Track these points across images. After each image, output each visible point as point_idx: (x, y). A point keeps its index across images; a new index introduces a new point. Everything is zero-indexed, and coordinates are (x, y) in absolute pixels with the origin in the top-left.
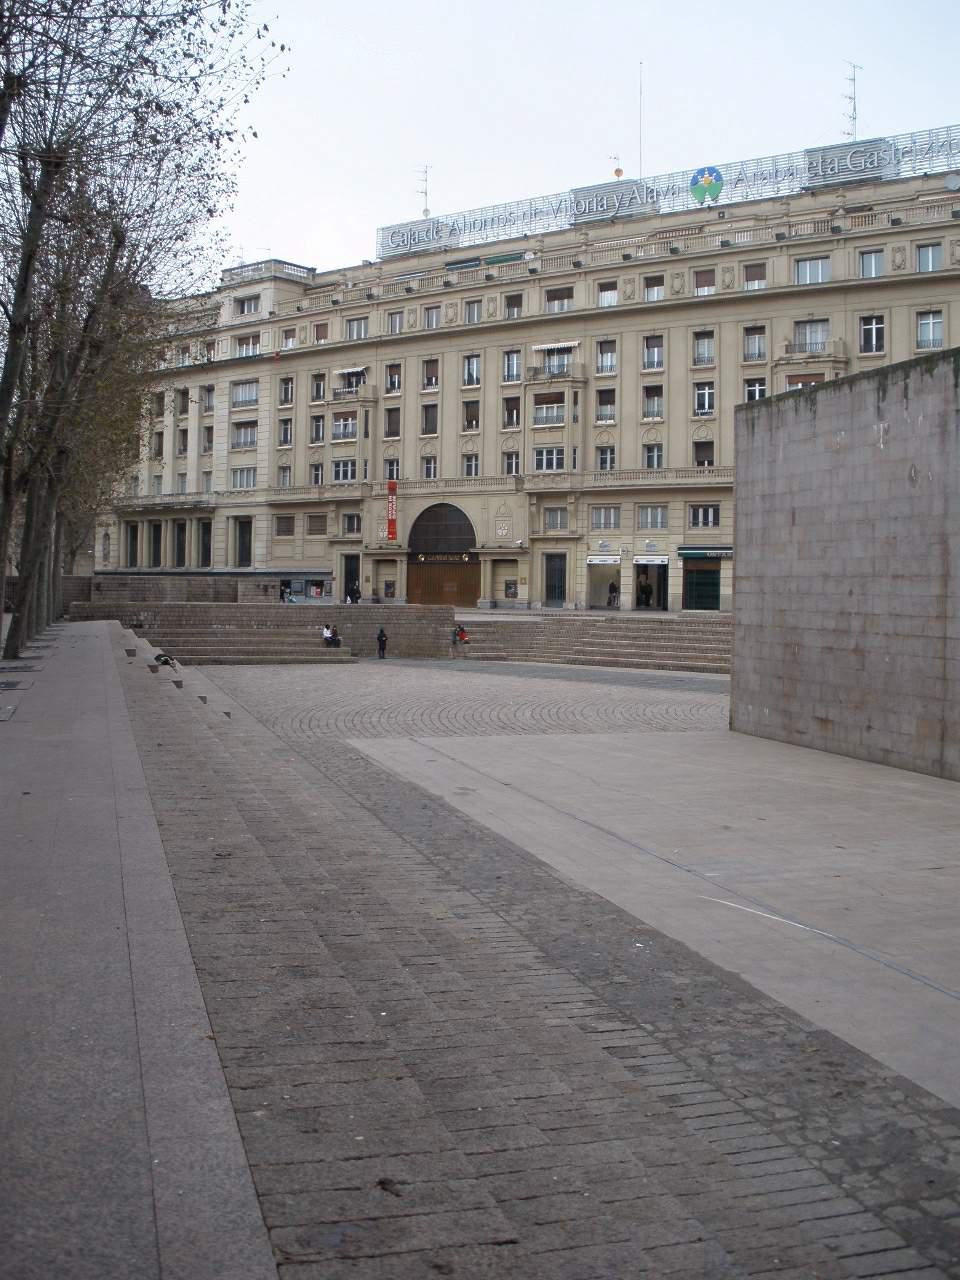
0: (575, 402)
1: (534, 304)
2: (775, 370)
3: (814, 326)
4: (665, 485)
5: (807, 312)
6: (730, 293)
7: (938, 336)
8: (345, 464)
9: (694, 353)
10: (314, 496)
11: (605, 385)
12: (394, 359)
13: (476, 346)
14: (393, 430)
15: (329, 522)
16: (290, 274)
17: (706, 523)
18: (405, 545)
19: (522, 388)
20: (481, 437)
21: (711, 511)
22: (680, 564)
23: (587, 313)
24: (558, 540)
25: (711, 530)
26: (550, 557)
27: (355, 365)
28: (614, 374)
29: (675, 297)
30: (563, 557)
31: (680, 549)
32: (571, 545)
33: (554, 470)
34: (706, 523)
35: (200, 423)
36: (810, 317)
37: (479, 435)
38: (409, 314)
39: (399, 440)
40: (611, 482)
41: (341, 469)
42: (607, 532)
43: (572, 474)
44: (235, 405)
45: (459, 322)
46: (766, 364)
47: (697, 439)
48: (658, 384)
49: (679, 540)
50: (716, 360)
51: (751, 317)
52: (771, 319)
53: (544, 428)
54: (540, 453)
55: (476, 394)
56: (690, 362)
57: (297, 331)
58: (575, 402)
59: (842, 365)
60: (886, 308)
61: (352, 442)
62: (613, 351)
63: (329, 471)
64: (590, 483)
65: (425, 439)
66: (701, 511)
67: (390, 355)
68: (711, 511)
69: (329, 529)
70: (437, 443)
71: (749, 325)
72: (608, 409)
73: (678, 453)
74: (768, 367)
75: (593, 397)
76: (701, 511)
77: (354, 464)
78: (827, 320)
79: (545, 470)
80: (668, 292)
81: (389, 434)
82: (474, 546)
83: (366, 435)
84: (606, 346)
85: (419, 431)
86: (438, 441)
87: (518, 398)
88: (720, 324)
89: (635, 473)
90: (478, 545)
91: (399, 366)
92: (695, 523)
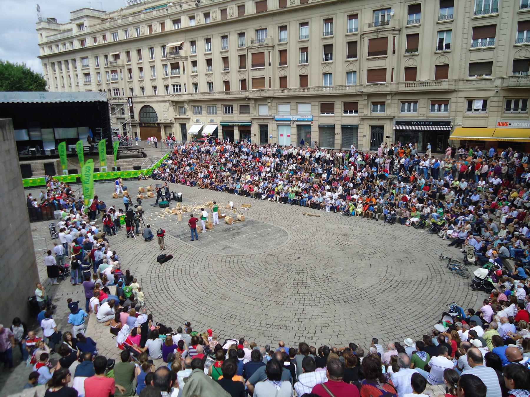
0: (121, 72)
1: (169, 26)
2: (363, 36)
3: (263, 31)
4: (289, 95)
5: (379, 4)
6: (233, 18)
7: (308, 34)
8: (177, 86)
9: (279, 37)
10: (243, 95)
11: (283, 48)
12: (208, 36)
13: (331, 13)
14: (284, 62)
15: (251, 108)
16: (96, 15)
17: (229, 113)
18: (138, 121)
19: (246, 50)
20: (358, 62)
21: (230, 107)
22: (221, 128)
23: (251, 16)
24: (379, 119)
25: (230, 115)
26: (373, 127)
27: (116, 52)
28: (308, 39)
29: (214, 21)
30: (266, 126)
31: (220, 122)
32: (270, 121)
33: (179, 93)
34: (229, 113)
35: (60, 76)
36: (382, 7)
37: (357, 60)
38: (230, 9)
39: (287, 67)
40: (197, 97)
41: (176, 88)
42: (213, 116)
43: (269, 90)
44: (83, 66)
45: (218, 20)
46: (358, 34)
47: (301, 74)
48: (210, 58)
49: (220, 119)
50: (288, 40)
51: (326, 13)
52: (229, 32)
53: (257, 69)
54: (174, 86)
55: (153, 63)
56: (237, 46)
57: (153, 26)
58: (121, 72)
59: (397, 32)
60: (309, 18)
61: (178, 76)
62: (286, 30)
63: (250, 84)
64: (277, 94)
65: (281, 67)
66: (227, 107)
67: (126, 47)
68: (230, 107)
69: (251, 112)
70: (287, 69)
71: (301, 22)
72: (195, 69)
73: (219, 87)
74: (359, 36)
75: (190, 64)
76: (227, 107)
77: (180, 86)
78: (266, 29)
79: (176, 93)
80: (196, 23)
81: (281, 64)
82: (157, 120)
83: (270, 65)
84: (283, 28)
85: (345, 57)
86: (333, 65)
87: (356, 42)
88: (229, 32)
89: (427, 83)
90: (159, 120)
91: (210, 39)
92: (226, 113)
